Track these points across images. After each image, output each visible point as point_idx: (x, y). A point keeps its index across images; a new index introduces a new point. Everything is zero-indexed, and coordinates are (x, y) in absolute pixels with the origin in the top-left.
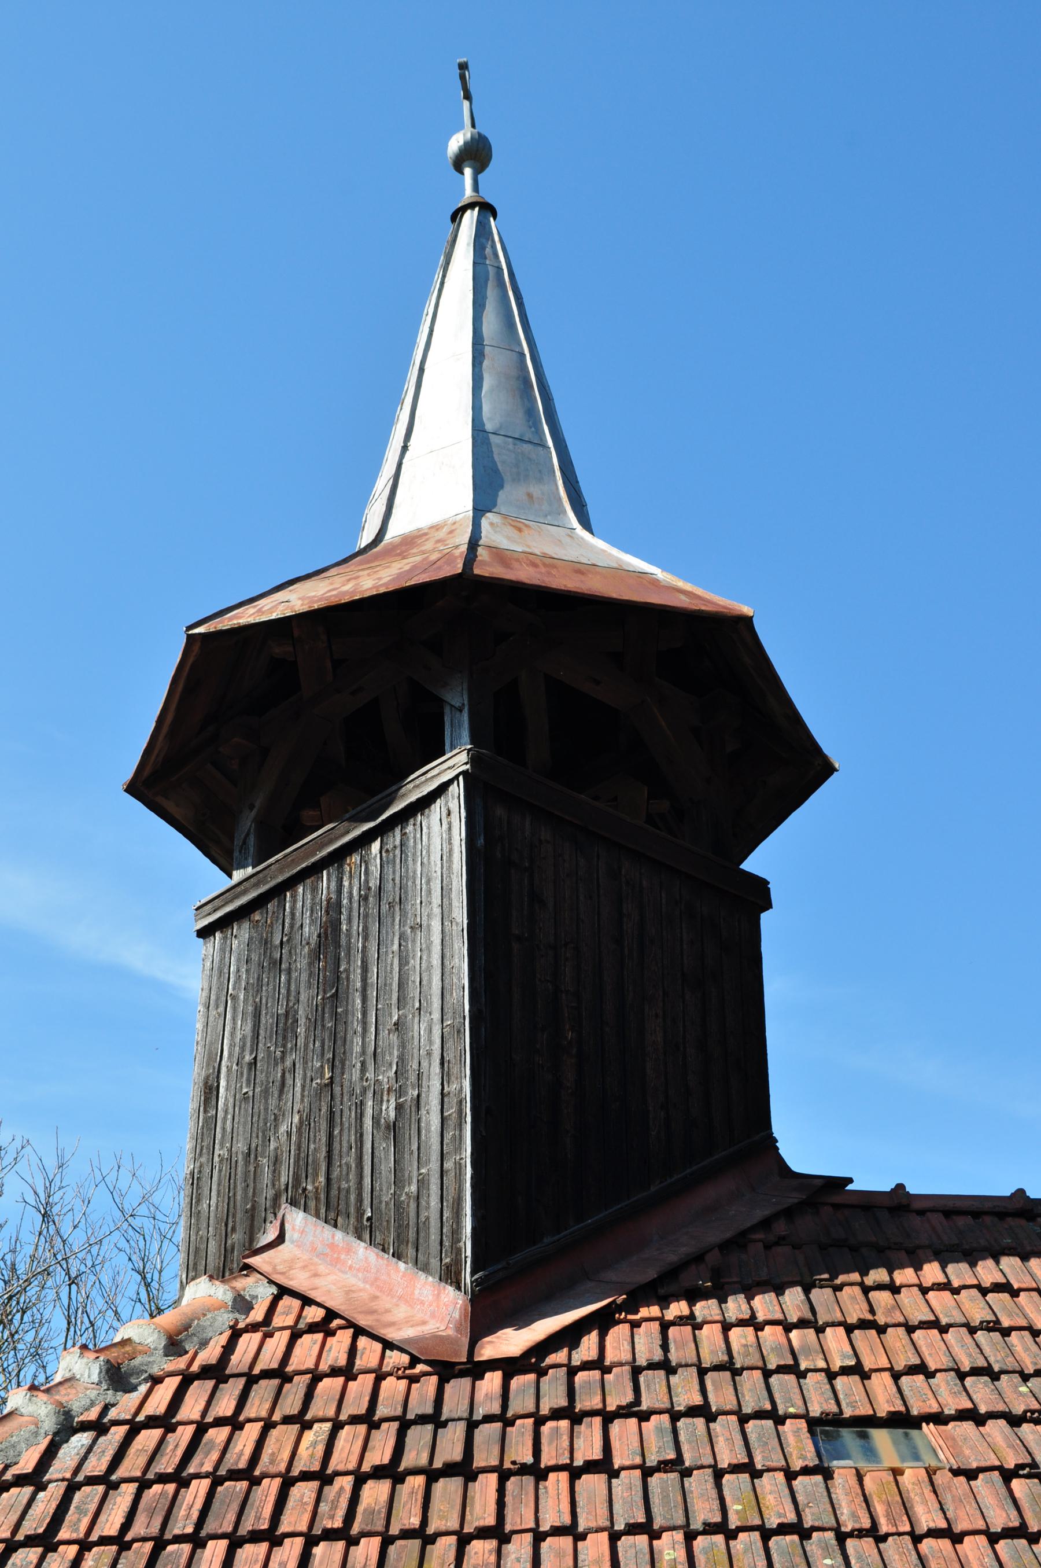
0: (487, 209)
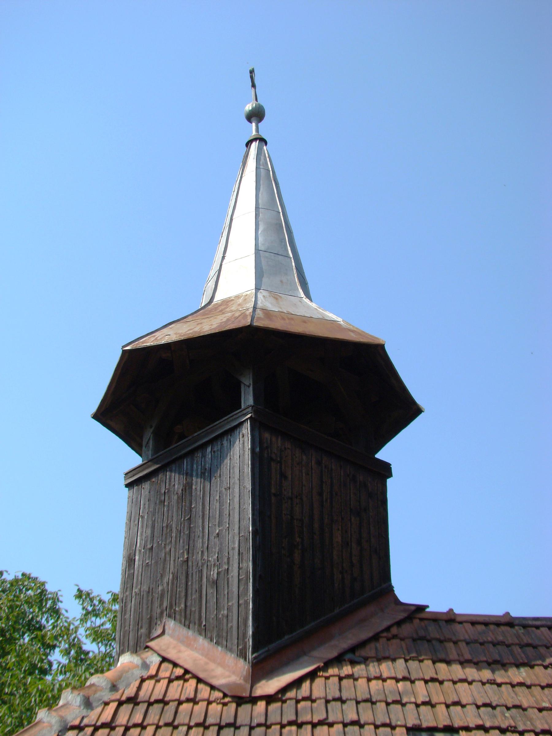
0: (263, 141)
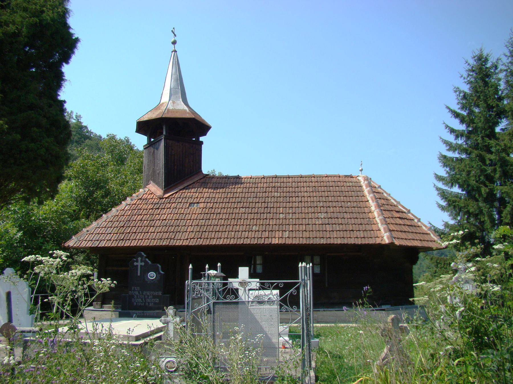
0: (175, 51)
